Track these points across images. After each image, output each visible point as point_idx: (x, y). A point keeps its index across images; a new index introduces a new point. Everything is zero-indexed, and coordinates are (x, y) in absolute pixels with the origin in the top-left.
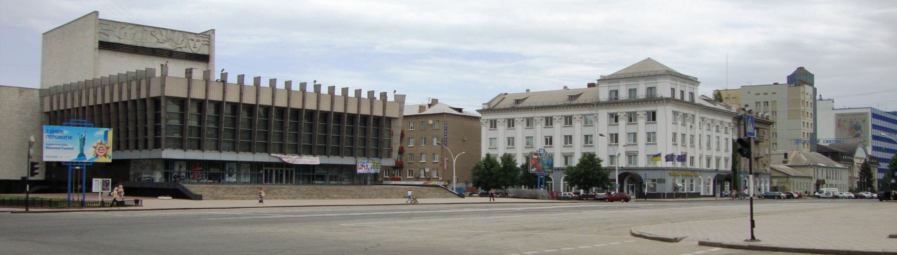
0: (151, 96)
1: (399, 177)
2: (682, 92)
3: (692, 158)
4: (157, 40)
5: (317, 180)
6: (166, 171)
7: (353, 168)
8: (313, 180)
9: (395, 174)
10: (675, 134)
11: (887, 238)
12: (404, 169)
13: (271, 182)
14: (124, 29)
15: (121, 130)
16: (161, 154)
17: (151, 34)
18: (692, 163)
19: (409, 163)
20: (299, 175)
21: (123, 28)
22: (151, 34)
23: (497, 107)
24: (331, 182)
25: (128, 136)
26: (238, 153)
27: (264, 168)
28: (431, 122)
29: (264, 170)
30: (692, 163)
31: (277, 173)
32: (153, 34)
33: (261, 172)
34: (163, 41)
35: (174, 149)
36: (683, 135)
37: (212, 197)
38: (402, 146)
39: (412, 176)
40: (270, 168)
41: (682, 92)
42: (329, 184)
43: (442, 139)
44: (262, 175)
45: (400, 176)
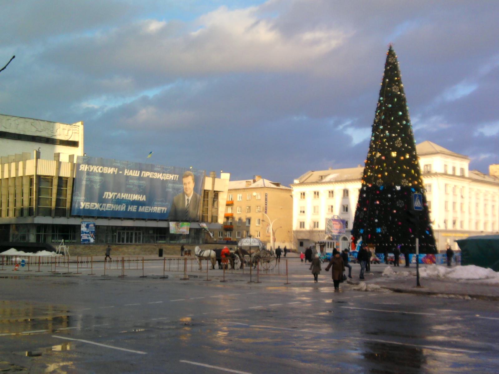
0: (27, 174)
1: (229, 237)
2: (454, 169)
3: (462, 222)
4: (36, 129)
5: (159, 240)
6: (37, 233)
7: (167, 229)
8: (157, 240)
9: (227, 235)
10: (446, 202)
11: (391, 47)
12: (233, 231)
13: (131, 242)
14: (9, 120)
15: (10, 200)
16: (33, 220)
17: (32, 124)
18: (462, 226)
19: (238, 226)
20: (54, 235)
21: (8, 120)
22: (32, 124)
23: (306, 182)
24: (171, 242)
25: (8, 206)
26: (134, 221)
27: (118, 231)
28: (254, 194)
29: (117, 233)
30: (462, 226)
31: (136, 234)
32: (33, 125)
33: (115, 234)
34: (41, 130)
35: (44, 216)
36: (454, 203)
37: (134, 253)
38: (232, 213)
39: (240, 236)
40: (131, 231)
41: (454, 169)
42: (170, 244)
43: (263, 208)
44: (116, 236)
45: (230, 236)
